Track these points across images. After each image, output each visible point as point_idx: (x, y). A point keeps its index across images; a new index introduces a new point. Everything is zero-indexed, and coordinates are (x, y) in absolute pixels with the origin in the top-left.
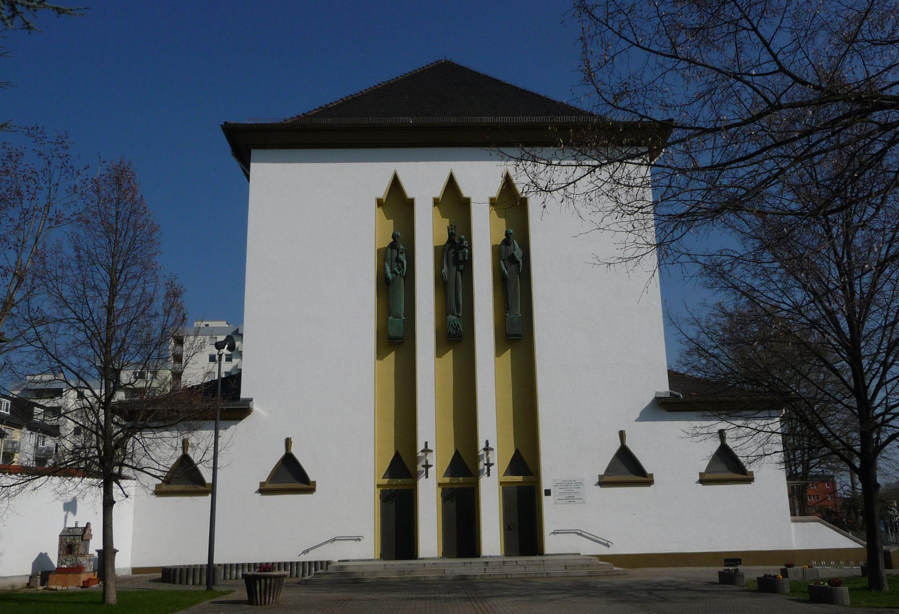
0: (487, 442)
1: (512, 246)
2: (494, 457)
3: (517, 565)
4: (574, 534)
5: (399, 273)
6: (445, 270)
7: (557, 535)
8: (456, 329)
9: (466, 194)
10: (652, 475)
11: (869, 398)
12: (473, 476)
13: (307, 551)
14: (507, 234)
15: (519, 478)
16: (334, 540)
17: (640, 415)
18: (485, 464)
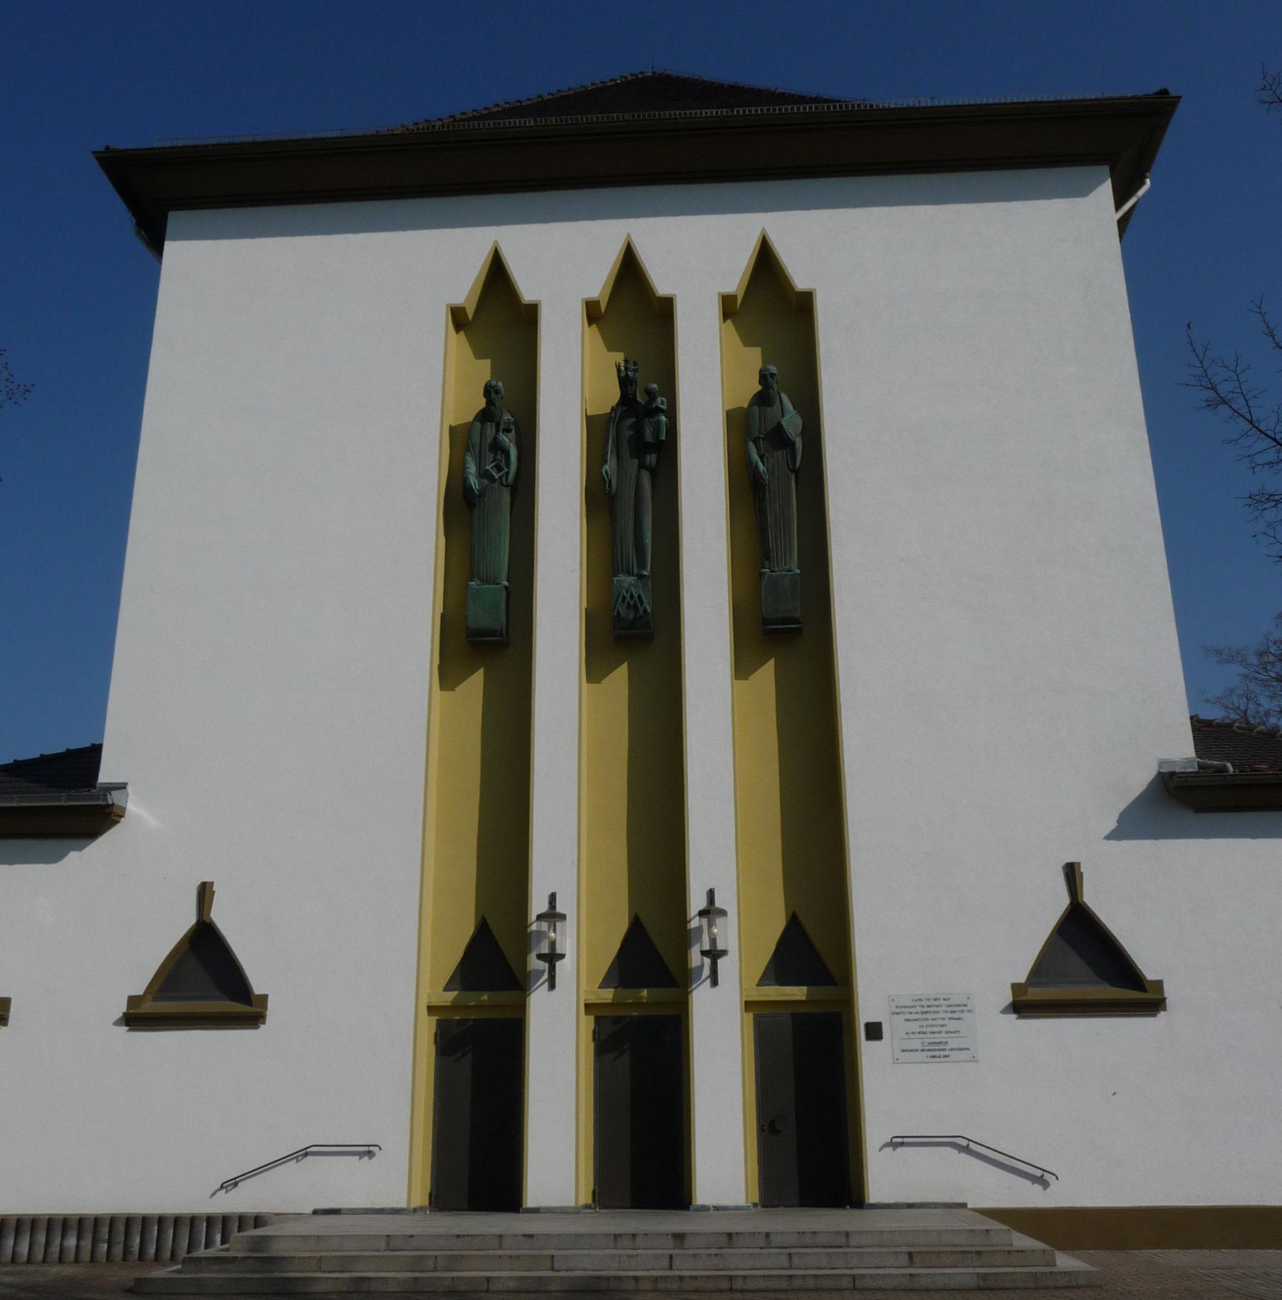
0: (711, 894)
1: (777, 407)
3: (769, 1245)
4: (949, 1149)
5: (497, 476)
6: (610, 467)
7: (899, 1149)
8: (635, 608)
9: (662, 287)
10: (1159, 984)
13: (234, 1183)
14: (764, 378)
15: (798, 993)
16: (305, 1153)
17: (1118, 821)
18: (704, 953)
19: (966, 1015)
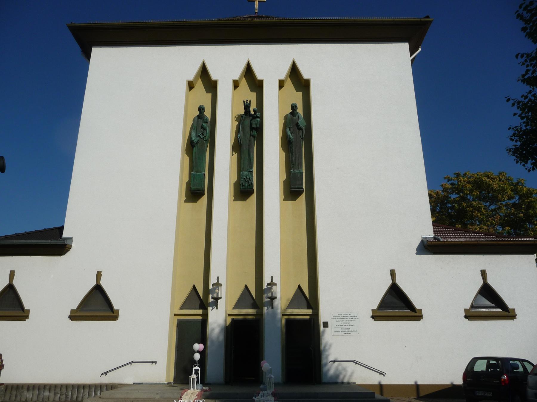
2: (222, 292)
4: (352, 362)
10: (421, 310)
11: (234, 152)
12: (260, 309)
16: (130, 363)
19: (356, 320)
